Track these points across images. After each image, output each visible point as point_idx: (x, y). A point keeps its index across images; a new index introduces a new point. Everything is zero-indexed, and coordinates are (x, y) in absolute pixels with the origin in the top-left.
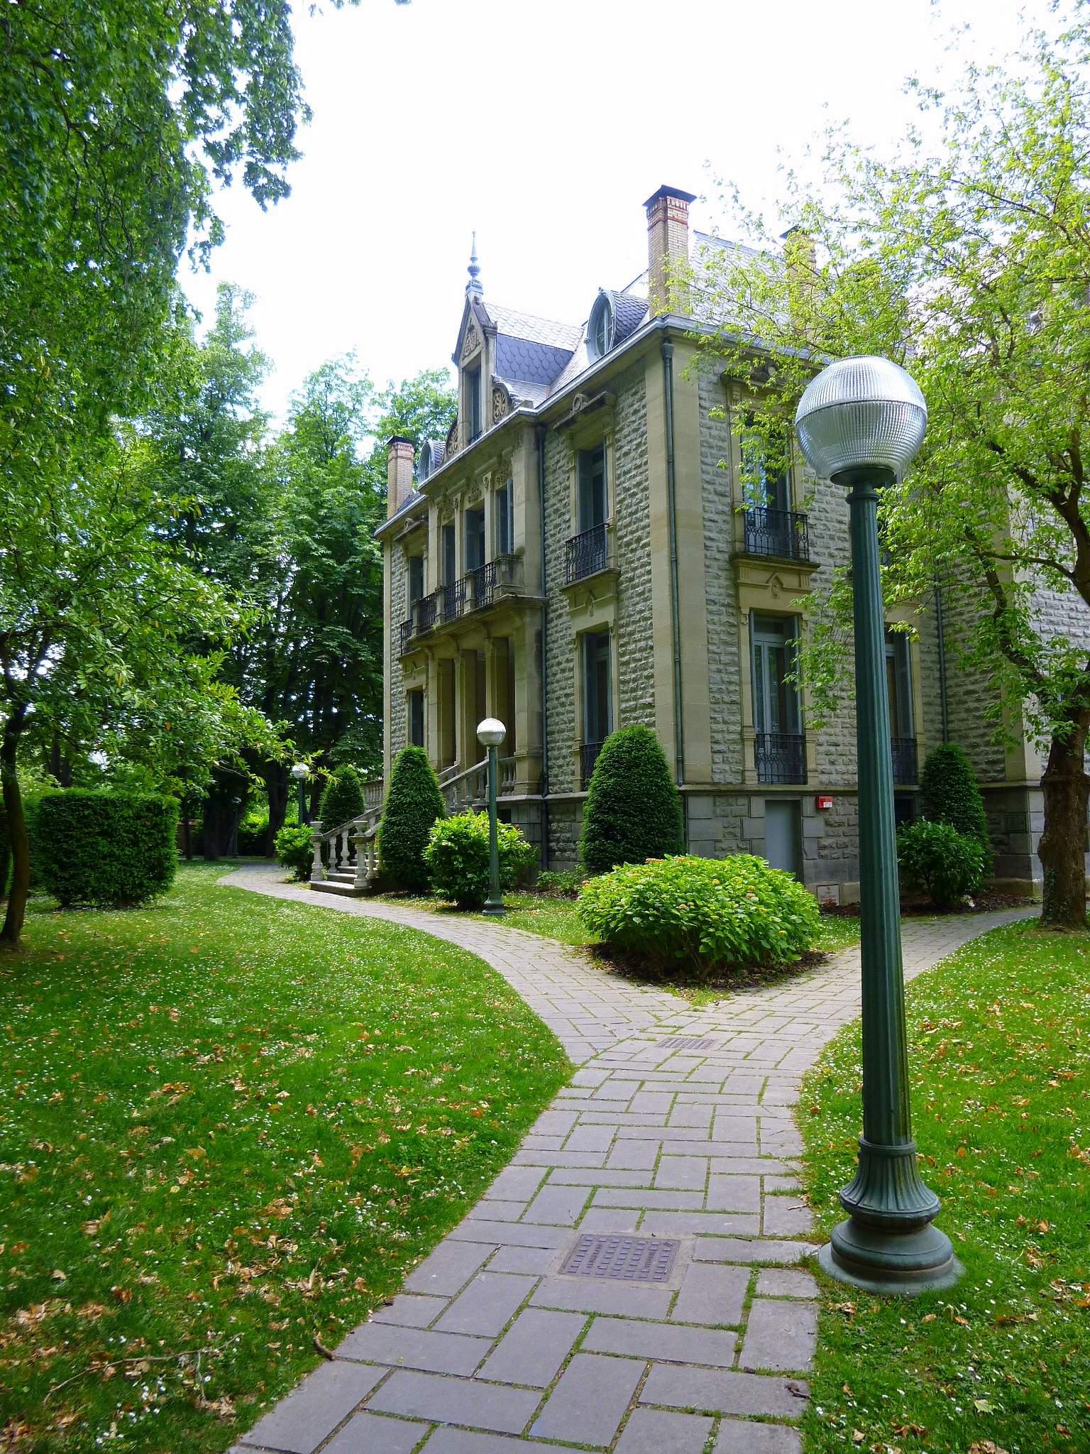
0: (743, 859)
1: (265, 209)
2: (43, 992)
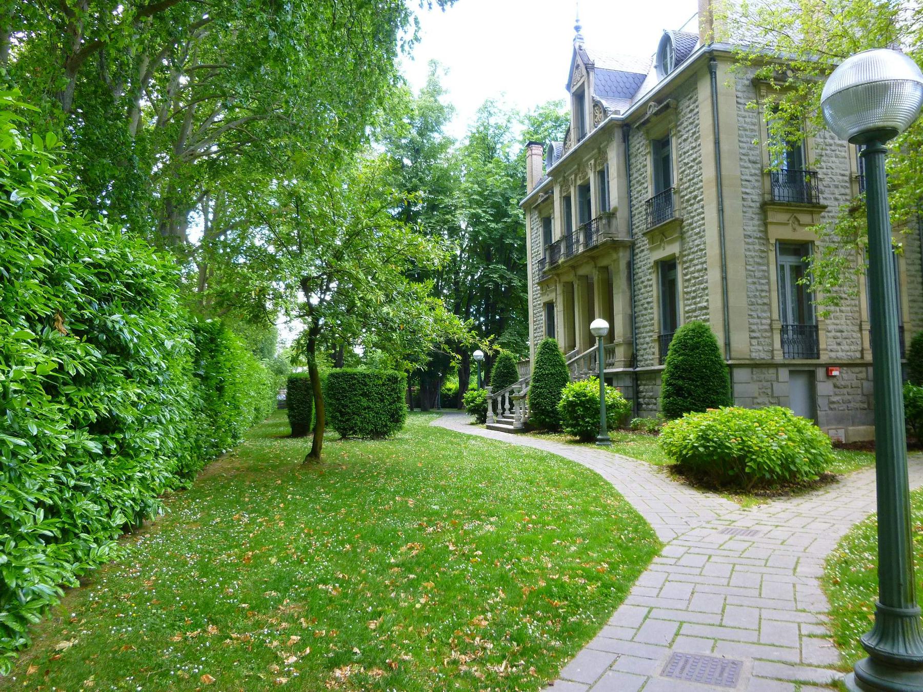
0: (776, 411)
1: (443, 10)
2: (335, 488)
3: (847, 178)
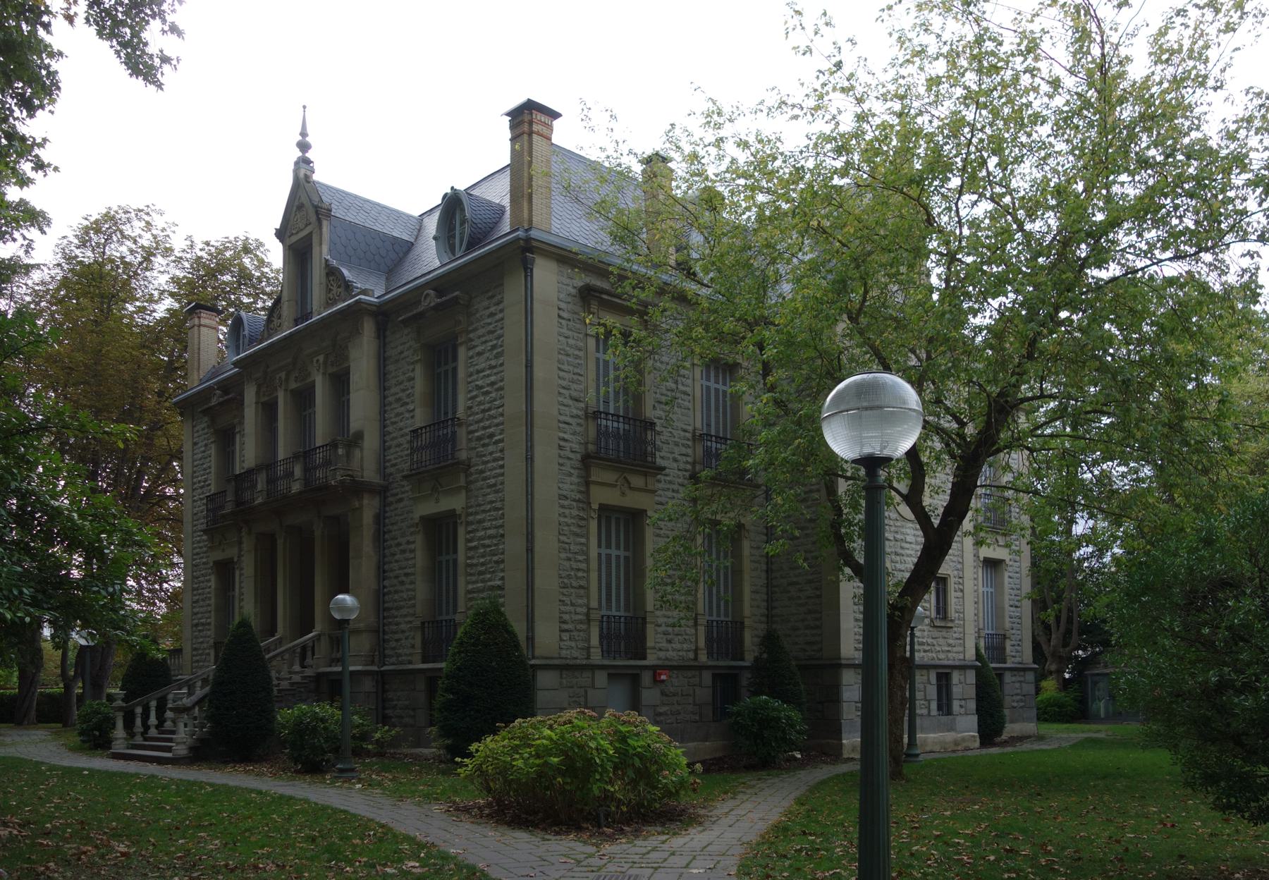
3: (689, 435)
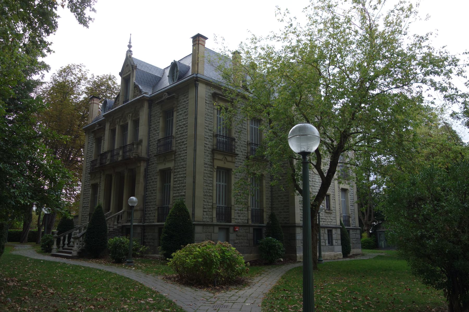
3: (246, 143)
